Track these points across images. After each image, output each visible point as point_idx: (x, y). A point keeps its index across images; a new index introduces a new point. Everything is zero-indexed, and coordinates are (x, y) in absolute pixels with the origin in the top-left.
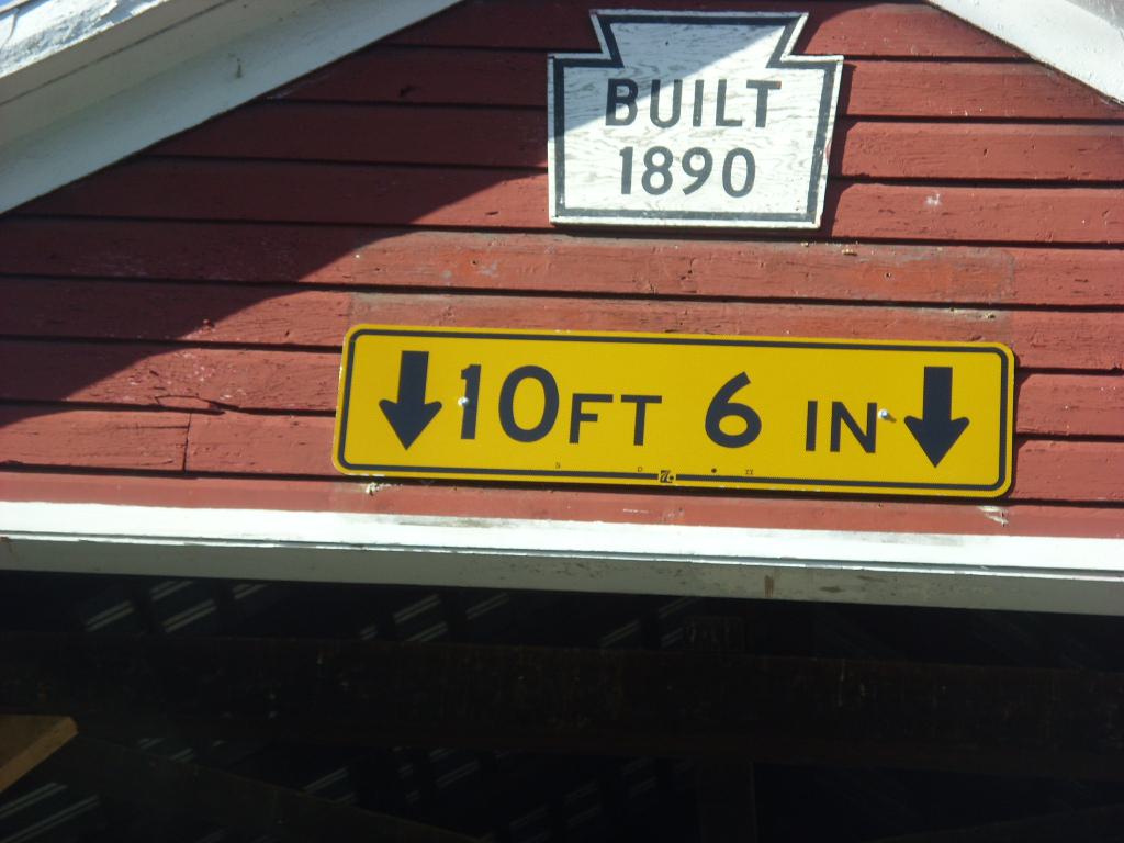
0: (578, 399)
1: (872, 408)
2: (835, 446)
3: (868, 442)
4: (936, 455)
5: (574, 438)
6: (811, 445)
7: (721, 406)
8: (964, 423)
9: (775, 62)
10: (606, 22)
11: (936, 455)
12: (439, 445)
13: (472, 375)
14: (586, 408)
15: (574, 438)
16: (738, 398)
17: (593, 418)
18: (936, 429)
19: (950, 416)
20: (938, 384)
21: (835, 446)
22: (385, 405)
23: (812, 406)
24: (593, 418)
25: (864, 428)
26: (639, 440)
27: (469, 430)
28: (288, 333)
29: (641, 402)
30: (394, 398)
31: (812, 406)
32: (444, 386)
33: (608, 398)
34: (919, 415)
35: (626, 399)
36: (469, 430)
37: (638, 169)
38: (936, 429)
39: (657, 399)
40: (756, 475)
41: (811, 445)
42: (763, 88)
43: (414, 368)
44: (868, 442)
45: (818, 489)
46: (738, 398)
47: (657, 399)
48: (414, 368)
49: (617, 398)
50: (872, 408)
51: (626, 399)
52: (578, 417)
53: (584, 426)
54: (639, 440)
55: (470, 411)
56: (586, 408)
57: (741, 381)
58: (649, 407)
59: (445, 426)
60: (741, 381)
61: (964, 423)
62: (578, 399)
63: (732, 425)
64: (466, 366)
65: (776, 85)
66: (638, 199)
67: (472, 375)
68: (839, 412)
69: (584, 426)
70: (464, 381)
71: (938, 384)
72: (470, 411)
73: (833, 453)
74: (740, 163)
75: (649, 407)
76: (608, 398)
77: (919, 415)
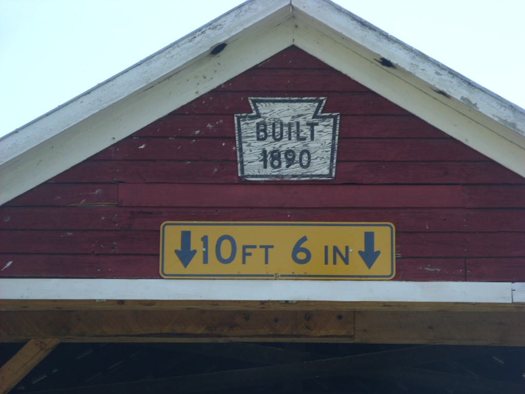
0: (245, 247)
1: (347, 248)
2: (335, 263)
3: (346, 261)
4: (185, 265)
5: (244, 262)
6: (326, 263)
7: (297, 248)
8: (378, 253)
9: (315, 116)
10: (254, 102)
11: (185, 265)
12: (196, 263)
13: (205, 239)
14: (248, 250)
15: (244, 262)
16: (303, 245)
17: (250, 254)
18: (369, 256)
19: (190, 249)
20: (369, 237)
21: (335, 263)
22: (360, 252)
23: (326, 248)
24: (250, 254)
25: (338, 255)
26: (266, 262)
27: (205, 261)
28: (445, 219)
29: (267, 248)
30: (179, 248)
31: (326, 248)
32: (196, 244)
33: (254, 247)
34: (363, 250)
35: (261, 247)
36: (205, 261)
37: (269, 158)
38: (369, 256)
39: (272, 247)
40: (308, 274)
41: (326, 263)
42: (312, 125)
43: (186, 237)
44: (346, 261)
45: (197, 277)
46: (303, 245)
47: (272, 247)
48: (186, 237)
49: (258, 247)
50: (347, 248)
51: (261, 247)
52: (245, 254)
53: (247, 257)
54: (266, 262)
55: (206, 255)
56: (248, 250)
57: (304, 239)
58: (269, 249)
59: (197, 259)
60: (304, 239)
61: (378, 253)
62: (245, 247)
63: (301, 256)
64: (202, 236)
65: (317, 124)
66: (269, 170)
67: (205, 239)
68: (336, 249)
69: (247, 257)
70: (202, 242)
71: (369, 237)
72: (206, 255)
73: (205, 265)
74: (305, 156)
75: (269, 249)
76: (254, 247)
77: (363, 250)
